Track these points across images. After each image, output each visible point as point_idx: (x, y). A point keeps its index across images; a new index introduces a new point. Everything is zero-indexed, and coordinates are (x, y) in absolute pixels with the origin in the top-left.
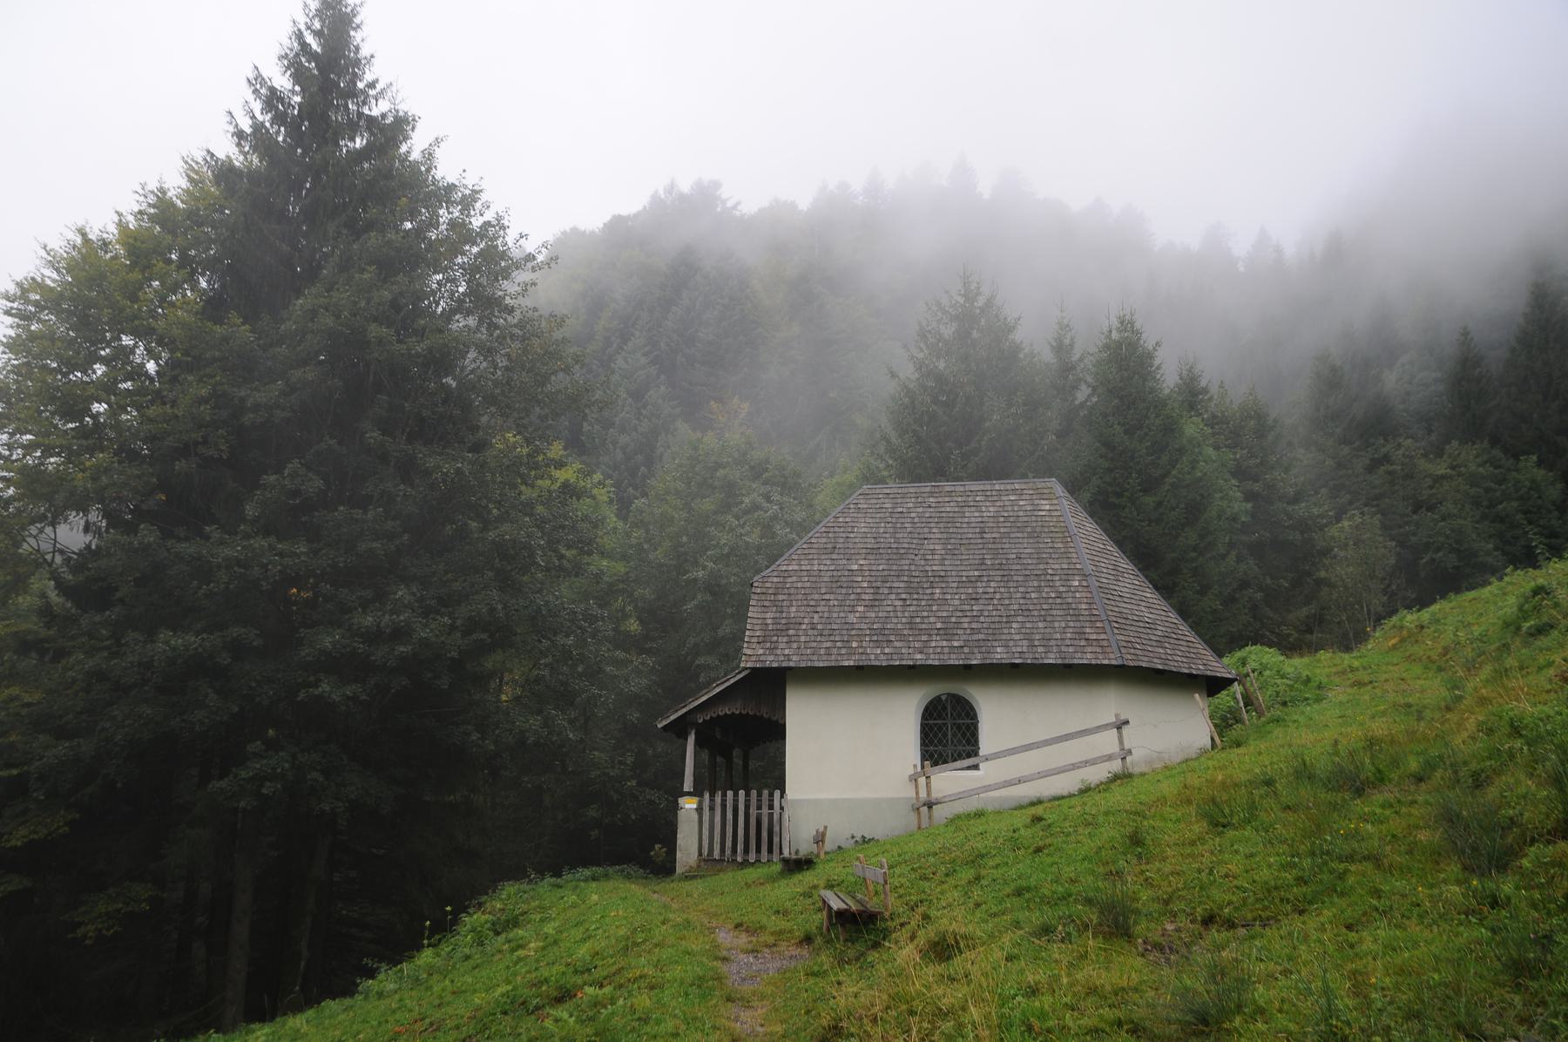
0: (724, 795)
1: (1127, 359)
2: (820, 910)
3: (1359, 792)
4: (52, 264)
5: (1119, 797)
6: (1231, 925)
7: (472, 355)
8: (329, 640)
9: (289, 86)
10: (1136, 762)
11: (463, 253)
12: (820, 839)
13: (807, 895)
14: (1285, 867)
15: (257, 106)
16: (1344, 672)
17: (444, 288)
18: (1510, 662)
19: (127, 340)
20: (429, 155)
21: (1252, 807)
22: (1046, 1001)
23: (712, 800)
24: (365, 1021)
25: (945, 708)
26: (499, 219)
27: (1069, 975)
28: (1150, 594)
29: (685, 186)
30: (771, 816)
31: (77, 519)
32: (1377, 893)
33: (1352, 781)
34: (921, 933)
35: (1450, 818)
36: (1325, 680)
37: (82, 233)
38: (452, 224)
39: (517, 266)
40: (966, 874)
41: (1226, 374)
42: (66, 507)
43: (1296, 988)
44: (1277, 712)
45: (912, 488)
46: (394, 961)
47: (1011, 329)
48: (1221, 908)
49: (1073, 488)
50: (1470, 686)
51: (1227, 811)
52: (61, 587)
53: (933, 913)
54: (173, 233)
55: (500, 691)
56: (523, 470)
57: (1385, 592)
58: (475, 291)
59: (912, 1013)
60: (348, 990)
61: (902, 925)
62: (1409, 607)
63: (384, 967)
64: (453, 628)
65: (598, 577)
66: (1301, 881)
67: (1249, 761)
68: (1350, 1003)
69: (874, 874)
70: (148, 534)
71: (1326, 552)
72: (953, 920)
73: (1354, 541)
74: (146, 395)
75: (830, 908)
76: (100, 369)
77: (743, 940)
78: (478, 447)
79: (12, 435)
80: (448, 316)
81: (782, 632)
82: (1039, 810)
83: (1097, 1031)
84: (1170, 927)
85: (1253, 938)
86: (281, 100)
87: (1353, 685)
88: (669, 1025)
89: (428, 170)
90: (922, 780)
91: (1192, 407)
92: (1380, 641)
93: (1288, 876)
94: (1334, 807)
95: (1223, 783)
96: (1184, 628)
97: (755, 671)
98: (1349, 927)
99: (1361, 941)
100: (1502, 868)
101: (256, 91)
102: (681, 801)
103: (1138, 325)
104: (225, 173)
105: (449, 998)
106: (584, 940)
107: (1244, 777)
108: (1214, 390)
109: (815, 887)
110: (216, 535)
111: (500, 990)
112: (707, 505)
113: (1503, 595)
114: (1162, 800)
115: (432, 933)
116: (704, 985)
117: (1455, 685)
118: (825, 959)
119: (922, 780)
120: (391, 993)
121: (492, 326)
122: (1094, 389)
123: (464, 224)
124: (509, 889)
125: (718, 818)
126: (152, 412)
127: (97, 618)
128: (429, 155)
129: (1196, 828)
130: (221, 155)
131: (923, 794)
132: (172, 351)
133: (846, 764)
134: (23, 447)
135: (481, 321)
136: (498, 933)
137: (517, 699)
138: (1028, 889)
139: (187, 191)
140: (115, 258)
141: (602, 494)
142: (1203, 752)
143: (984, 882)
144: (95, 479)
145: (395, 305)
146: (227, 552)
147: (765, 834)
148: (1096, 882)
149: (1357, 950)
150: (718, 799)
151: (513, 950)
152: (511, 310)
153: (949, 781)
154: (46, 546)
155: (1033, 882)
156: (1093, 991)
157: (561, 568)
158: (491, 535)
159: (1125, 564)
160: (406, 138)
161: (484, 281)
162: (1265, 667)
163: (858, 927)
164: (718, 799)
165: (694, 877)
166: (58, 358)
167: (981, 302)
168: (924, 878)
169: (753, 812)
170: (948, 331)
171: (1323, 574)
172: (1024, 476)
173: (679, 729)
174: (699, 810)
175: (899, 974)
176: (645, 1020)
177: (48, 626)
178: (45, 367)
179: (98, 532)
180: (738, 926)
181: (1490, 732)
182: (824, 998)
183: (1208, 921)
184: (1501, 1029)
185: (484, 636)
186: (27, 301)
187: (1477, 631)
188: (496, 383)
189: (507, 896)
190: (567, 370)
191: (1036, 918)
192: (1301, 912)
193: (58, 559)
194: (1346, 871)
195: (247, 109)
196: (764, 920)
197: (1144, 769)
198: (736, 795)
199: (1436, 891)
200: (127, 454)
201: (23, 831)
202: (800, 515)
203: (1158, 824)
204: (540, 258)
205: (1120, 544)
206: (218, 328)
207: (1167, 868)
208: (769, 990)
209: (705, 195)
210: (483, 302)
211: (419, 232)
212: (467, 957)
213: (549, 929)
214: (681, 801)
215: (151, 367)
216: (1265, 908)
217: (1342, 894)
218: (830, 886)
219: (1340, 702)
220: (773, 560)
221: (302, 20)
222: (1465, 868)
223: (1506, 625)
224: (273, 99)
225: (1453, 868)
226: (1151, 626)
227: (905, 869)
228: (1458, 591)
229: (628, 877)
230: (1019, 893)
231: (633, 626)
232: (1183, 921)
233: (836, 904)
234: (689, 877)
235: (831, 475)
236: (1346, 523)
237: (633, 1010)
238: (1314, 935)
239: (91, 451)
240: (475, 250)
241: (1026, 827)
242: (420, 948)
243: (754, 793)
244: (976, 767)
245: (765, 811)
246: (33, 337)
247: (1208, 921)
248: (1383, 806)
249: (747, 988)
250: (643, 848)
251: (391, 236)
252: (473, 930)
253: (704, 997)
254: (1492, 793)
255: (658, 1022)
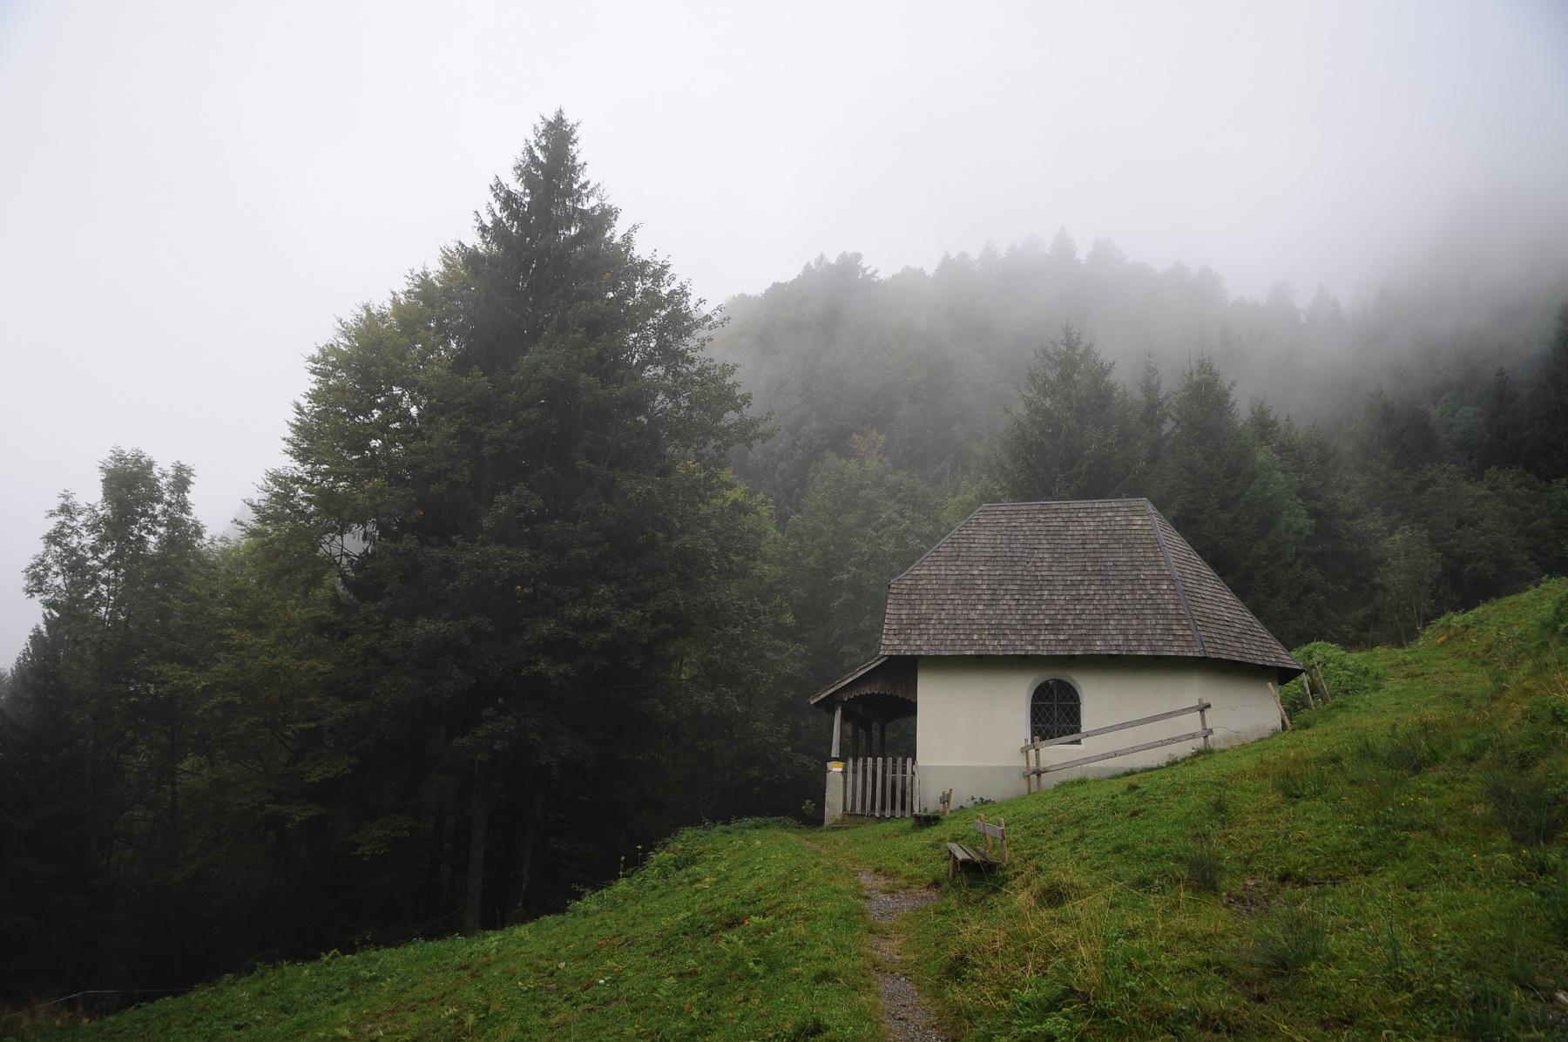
0: (865, 761)
1: (1206, 395)
2: (947, 859)
3: (1417, 770)
4: (345, 334)
5: (1203, 769)
6: (1304, 882)
7: (660, 398)
8: (546, 627)
9: (521, 189)
10: (1218, 739)
11: (654, 316)
12: (946, 799)
13: (935, 846)
14: (1351, 833)
15: (497, 206)
16: (1398, 665)
17: (638, 342)
18: (1549, 658)
19: (397, 391)
20: (627, 239)
21: (1322, 780)
22: (1145, 943)
23: (855, 765)
24: (574, 934)
25: (1052, 692)
26: (683, 287)
27: (1163, 921)
28: (1229, 597)
29: (832, 259)
30: (904, 779)
31: (358, 530)
32: (1435, 858)
33: (1410, 759)
34: (1034, 882)
35: (1499, 795)
36: (1381, 672)
37: (367, 309)
38: (646, 293)
39: (697, 325)
40: (1071, 833)
41: (1299, 410)
42: (350, 521)
43: (1365, 939)
44: (1339, 699)
45: (1024, 506)
46: (596, 887)
47: (1107, 373)
48: (1296, 867)
49: (1161, 506)
50: (1513, 678)
51: (1299, 783)
52: (346, 580)
53: (1043, 864)
54: (432, 306)
55: (680, 672)
56: (701, 491)
57: (1432, 596)
58: (663, 346)
59: (1029, 949)
60: (560, 909)
61: (1017, 874)
62: (1455, 610)
63: (588, 891)
64: (643, 619)
65: (761, 579)
66: (1366, 846)
67: (1317, 740)
68: (1414, 953)
69: (993, 830)
70: (409, 542)
71: (1381, 561)
72: (1067, 873)
73: (1400, 550)
74: (411, 432)
75: (955, 858)
76: (377, 413)
77: (882, 882)
78: (664, 473)
79: (314, 465)
80: (642, 366)
81: (912, 626)
82: (1133, 780)
83: (1188, 970)
84: (1250, 883)
85: (1325, 894)
86: (515, 200)
87: (1407, 677)
88: (822, 951)
89: (627, 251)
90: (1032, 752)
91: (1263, 437)
92: (1429, 639)
93: (1356, 842)
94: (1394, 782)
95: (1295, 760)
96: (1258, 626)
97: (892, 660)
98: (1410, 887)
99: (1421, 899)
100: (1548, 839)
101: (496, 195)
102: (829, 765)
103: (1215, 368)
104: (471, 259)
105: (640, 919)
106: (750, 878)
107: (1313, 755)
108: (1282, 422)
109: (942, 840)
110: (460, 543)
111: (682, 916)
112: (851, 519)
113: (1540, 600)
114: (1242, 774)
115: (628, 864)
116: (851, 918)
117: (1498, 678)
118: (952, 900)
119: (1032, 752)
120: (593, 915)
121: (677, 374)
122: (1178, 422)
123: (655, 293)
124: (688, 833)
125: (860, 781)
126: (414, 446)
127: (372, 607)
128: (627, 239)
129: (1273, 798)
130: (469, 245)
131: (1033, 764)
132: (430, 399)
133: (968, 737)
134: (321, 474)
135: (668, 370)
136: (679, 869)
137: (693, 678)
138: (1127, 847)
139: (443, 274)
140: (390, 327)
141: (764, 511)
142: (1275, 733)
143: (1087, 840)
144: (371, 499)
145: (600, 359)
146: (469, 556)
147: (899, 794)
148: (1179, 837)
149: (1418, 907)
150: (860, 764)
151: (692, 883)
152: (692, 361)
153: (1055, 753)
154: (336, 551)
155: (1130, 841)
156: (1184, 935)
157: (730, 571)
158: (675, 544)
159: (1206, 571)
160: (611, 226)
161: (670, 338)
162: (1328, 660)
163: (980, 874)
164: (860, 764)
165: (839, 829)
166: (347, 405)
167: (1081, 349)
168: (1035, 835)
169: (889, 775)
170: (1053, 375)
171: (1377, 580)
172: (1118, 496)
173: (828, 705)
174: (844, 773)
175: (1017, 915)
176: (802, 946)
177: (336, 612)
178: (338, 412)
179: (373, 541)
180: (877, 871)
181: (1534, 719)
182: (950, 932)
183: (1284, 878)
184: (1552, 981)
185: (668, 626)
186: (327, 363)
187: (1517, 631)
188: (680, 420)
189: (687, 839)
190: (738, 409)
191: (1137, 871)
192: (1367, 873)
193: (345, 561)
194: (1407, 839)
195: (487, 207)
196: (899, 866)
197: (1223, 746)
198: (875, 761)
199: (1488, 858)
200: (396, 480)
201: (319, 771)
202: (928, 529)
203: (1239, 794)
204: (715, 318)
205: (1200, 553)
206: (463, 380)
207: (1248, 833)
208: (904, 925)
209: (847, 268)
210: (670, 355)
211: (619, 300)
212: (655, 887)
213: (721, 867)
214: (829, 765)
215: (414, 411)
216: (1335, 869)
217: (1403, 859)
218: (955, 840)
219: (1399, 690)
220: (906, 565)
221: (532, 139)
222: (1514, 839)
223: (1544, 625)
224: (509, 200)
225: (1504, 839)
226: (1230, 624)
227: (1019, 827)
228: (1499, 596)
229: (785, 826)
230: (1118, 850)
231: (789, 619)
232: (1262, 878)
233: (961, 855)
234: (835, 828)
235: (954, 495)
236: (1397, 537)
237: (791, 937)
238: (1379, 894)
239: (369, 476)
240: (663, 313)
241: (1123, 794)
242: (616, 877)
243: (890, 760)
244: (1078, 742)
245: (899, 775)
246: (330, 389)
247: (1284, 878)
248: (1438, 783)
249: (885, 922)
250: (797, 802)
251: (597, 303)
252: (659, 865)
253: (849, 928)
254: (1538, 772)
255: (812, 947)
